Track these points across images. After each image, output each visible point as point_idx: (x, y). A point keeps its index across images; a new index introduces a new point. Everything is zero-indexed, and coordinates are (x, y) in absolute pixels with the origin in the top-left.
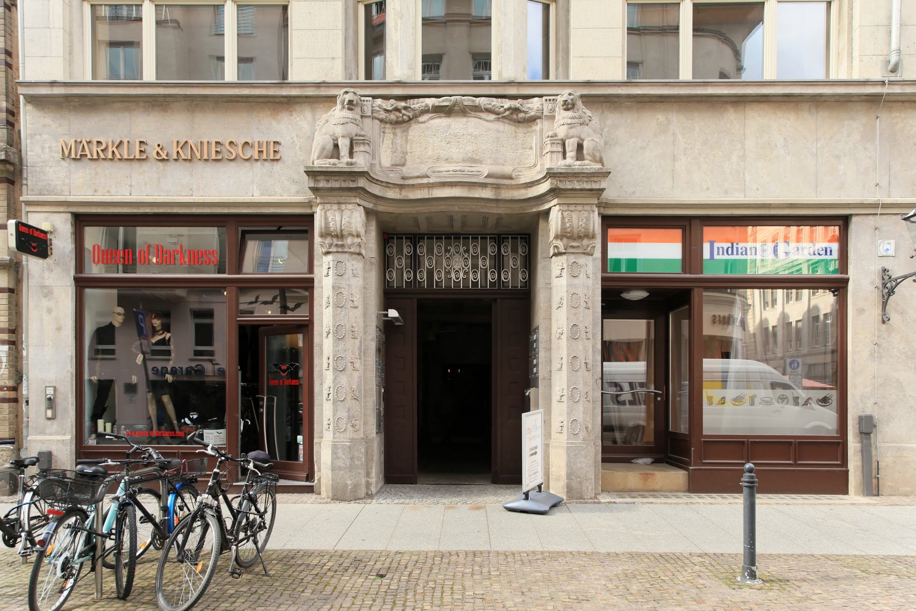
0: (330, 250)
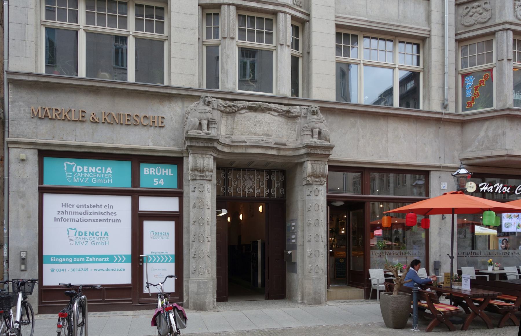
0: (196, 178)
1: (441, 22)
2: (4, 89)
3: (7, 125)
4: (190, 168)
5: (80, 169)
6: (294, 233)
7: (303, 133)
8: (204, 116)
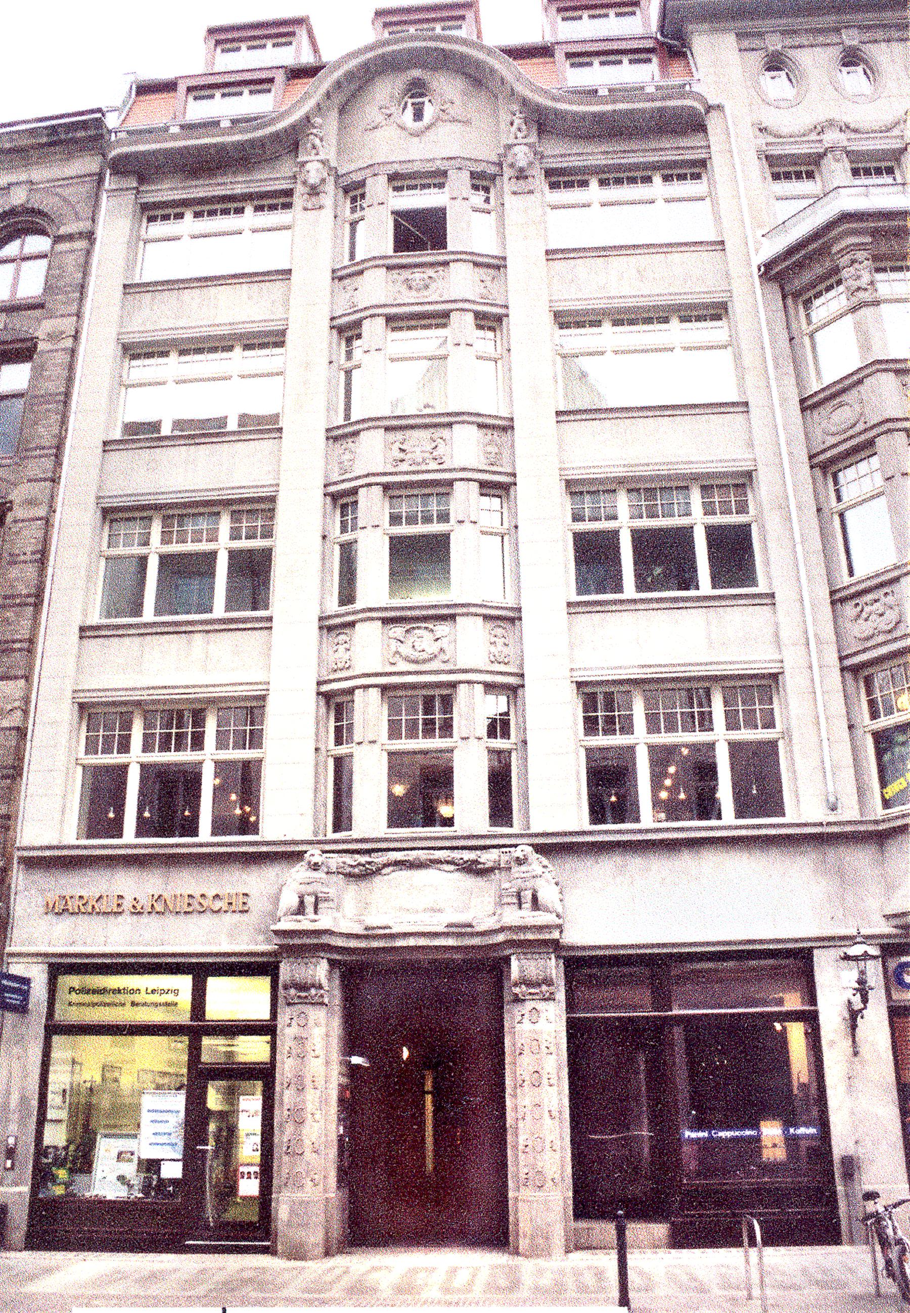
8: (310, 889)
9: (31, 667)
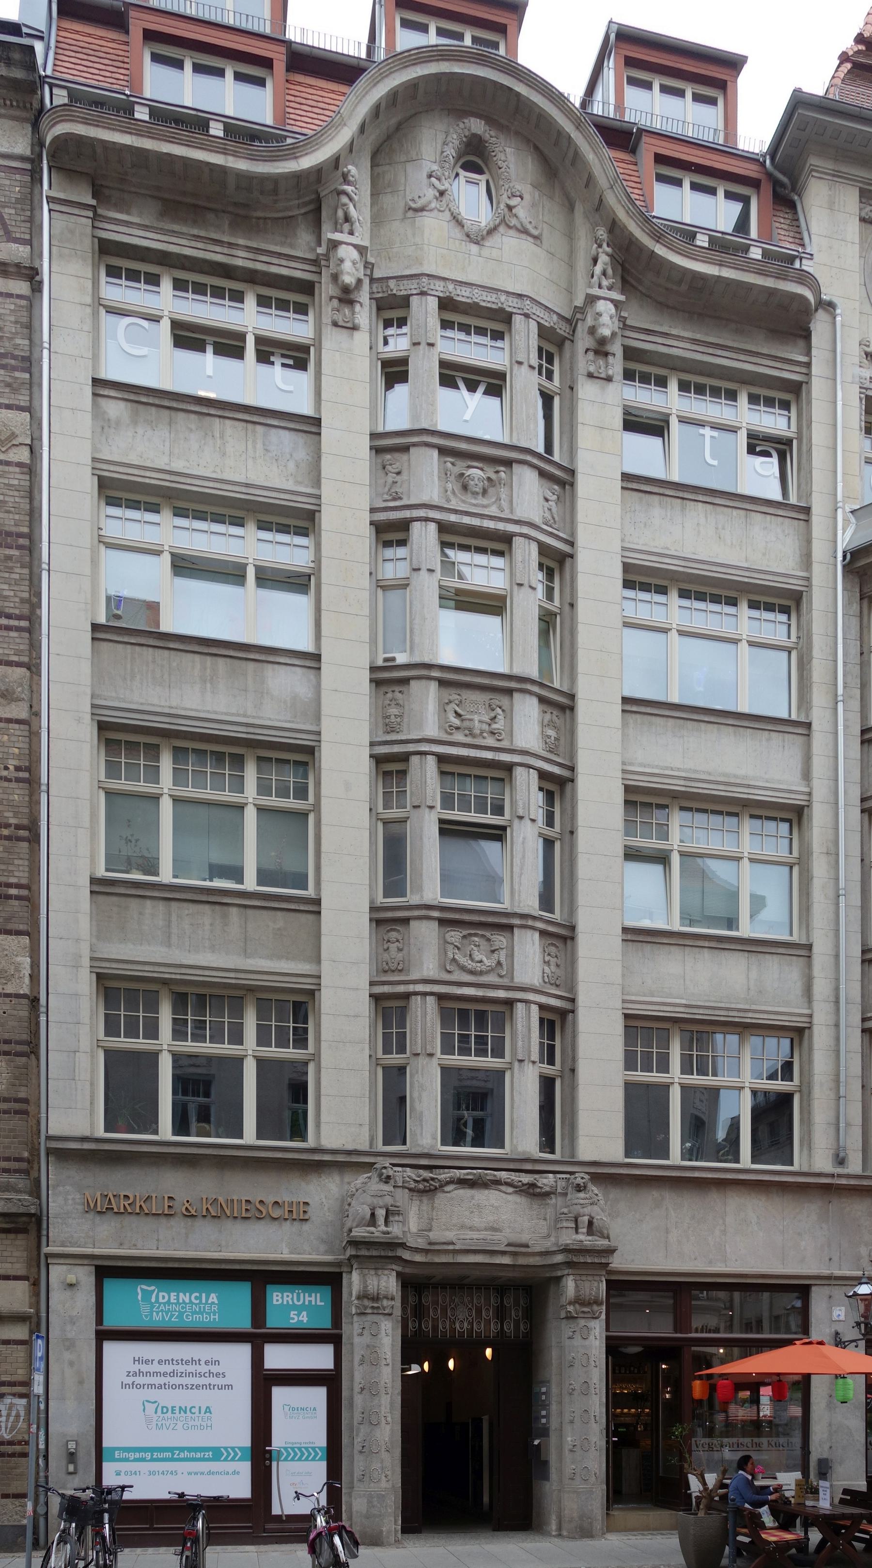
1: (832, 999)
2: (39, 1163)
3: (44, 1226)
4: (354, 1293)
5: (164, 1297)
6: (546, 1406)
7: (559, 1226)
9: (34, 646)
